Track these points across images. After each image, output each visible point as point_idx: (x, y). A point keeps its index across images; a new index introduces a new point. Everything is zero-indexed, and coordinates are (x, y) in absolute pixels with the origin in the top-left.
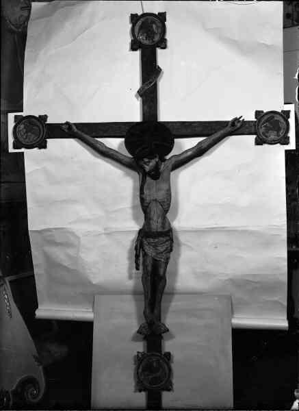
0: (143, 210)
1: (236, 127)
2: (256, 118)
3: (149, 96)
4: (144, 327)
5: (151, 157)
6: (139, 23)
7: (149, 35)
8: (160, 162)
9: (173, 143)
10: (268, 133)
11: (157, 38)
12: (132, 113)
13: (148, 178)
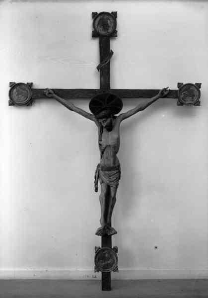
1: (166, 94)
3: (104, 69)
6: (98, 19)
7: (105, 28)
11: (110, 30)
12: (93, 83)
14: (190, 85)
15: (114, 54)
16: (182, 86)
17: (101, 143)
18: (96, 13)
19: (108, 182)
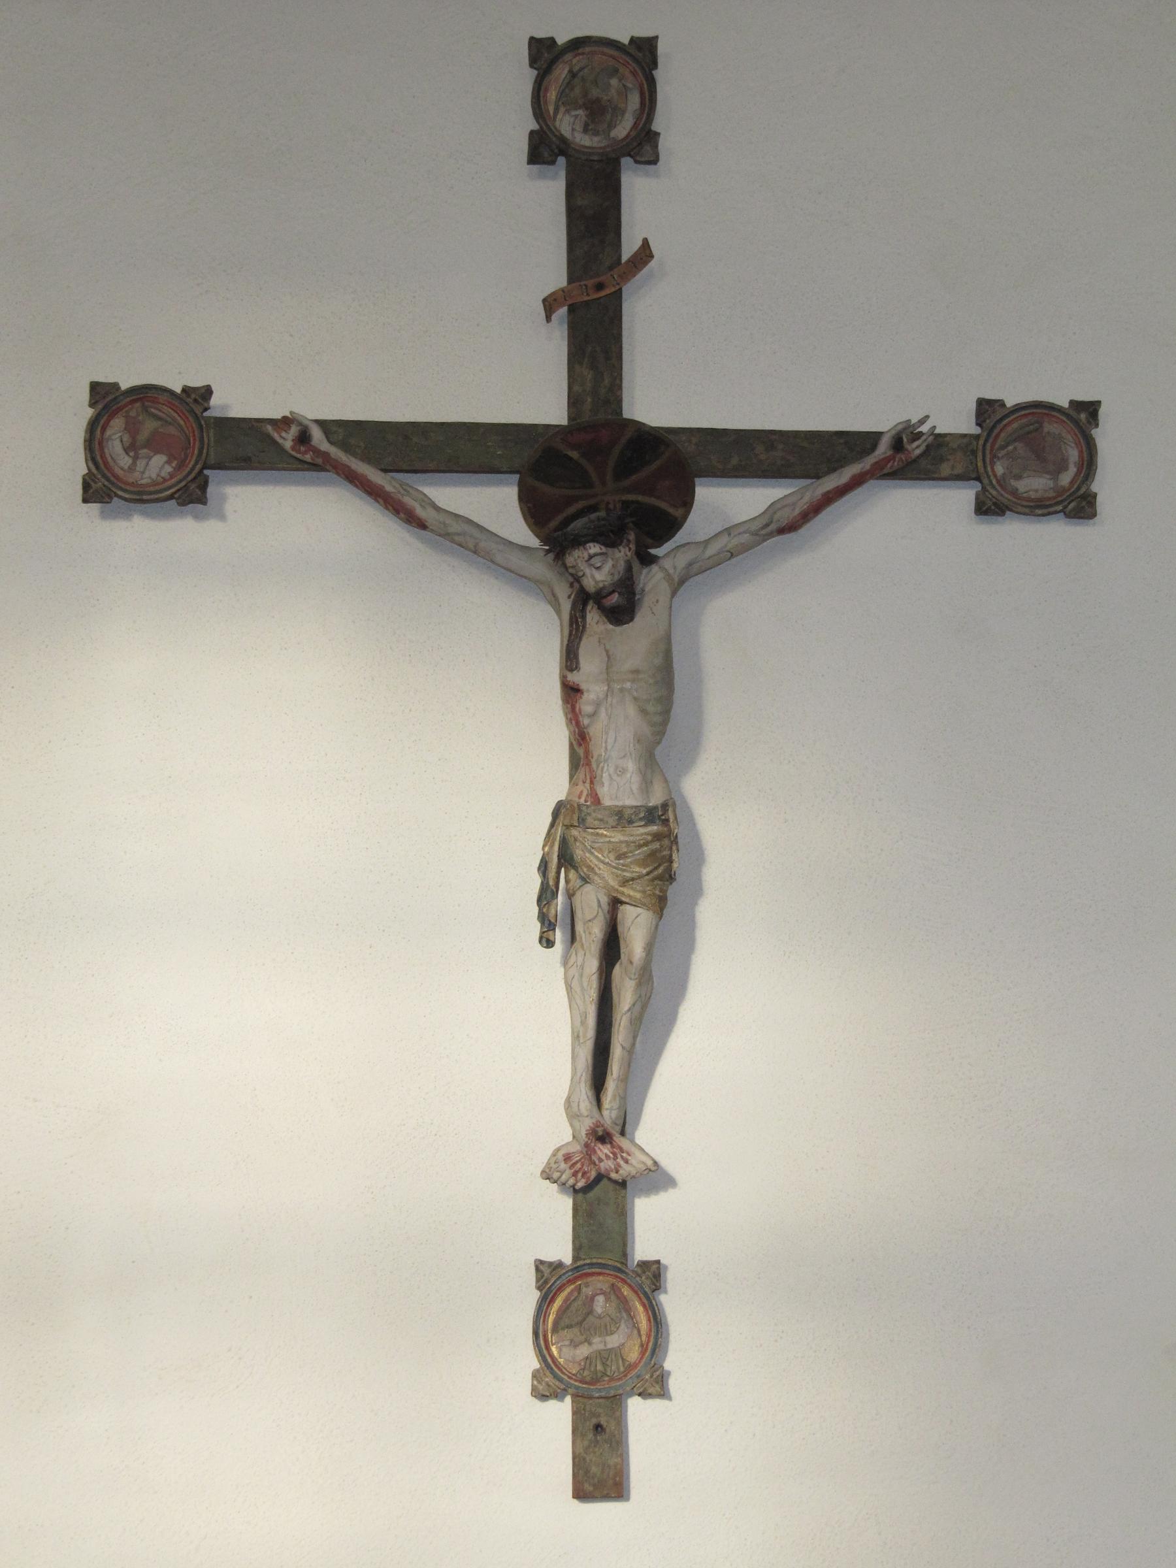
0: (566, 983)
1: (912, 457)
2: (979, 424)
3: (592, 317)
4: (567, 1158)
5: (610, 537)
6: (561, 72)
7: (594, 118)
8: (636, 565)
9: (687, 502)
10: (1019, 477)
11: (623, 129)
12: (531, 389)
13: (593, 616)
14: (1040, 410)
15: (653, 264)
16: (1003, 412)
17: (573, 678)
18: (552, 41)
19: (613, 883)
